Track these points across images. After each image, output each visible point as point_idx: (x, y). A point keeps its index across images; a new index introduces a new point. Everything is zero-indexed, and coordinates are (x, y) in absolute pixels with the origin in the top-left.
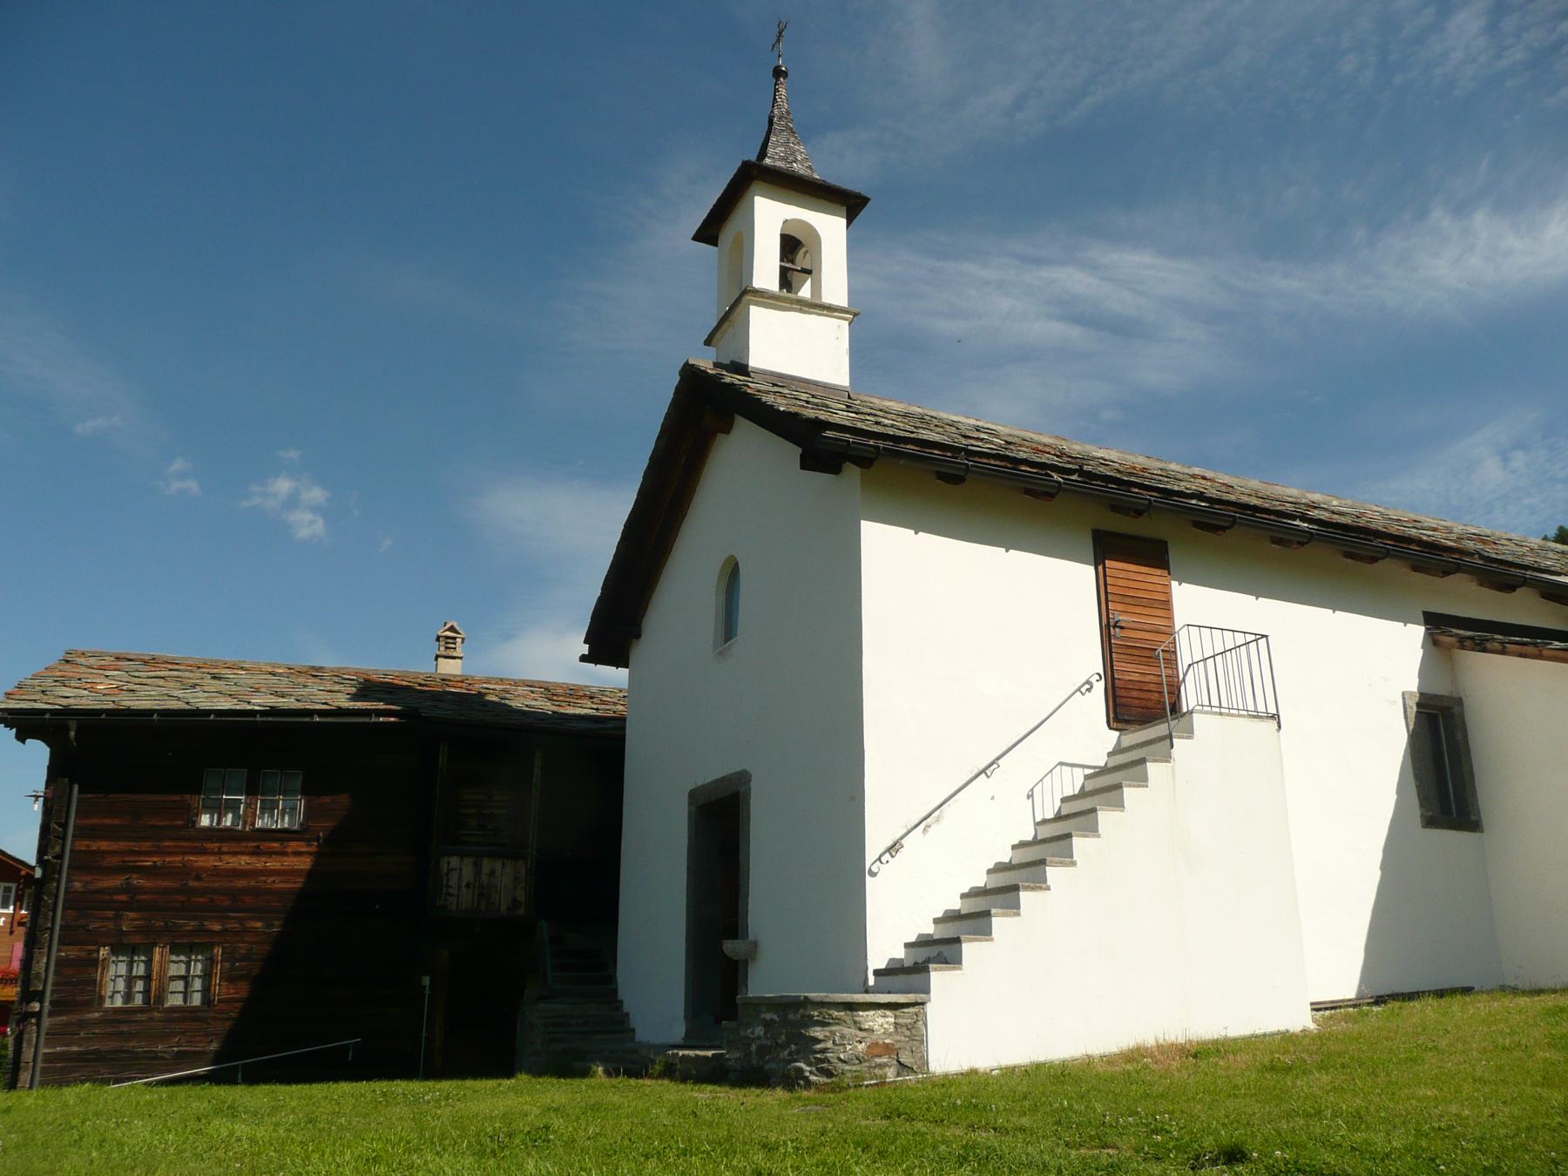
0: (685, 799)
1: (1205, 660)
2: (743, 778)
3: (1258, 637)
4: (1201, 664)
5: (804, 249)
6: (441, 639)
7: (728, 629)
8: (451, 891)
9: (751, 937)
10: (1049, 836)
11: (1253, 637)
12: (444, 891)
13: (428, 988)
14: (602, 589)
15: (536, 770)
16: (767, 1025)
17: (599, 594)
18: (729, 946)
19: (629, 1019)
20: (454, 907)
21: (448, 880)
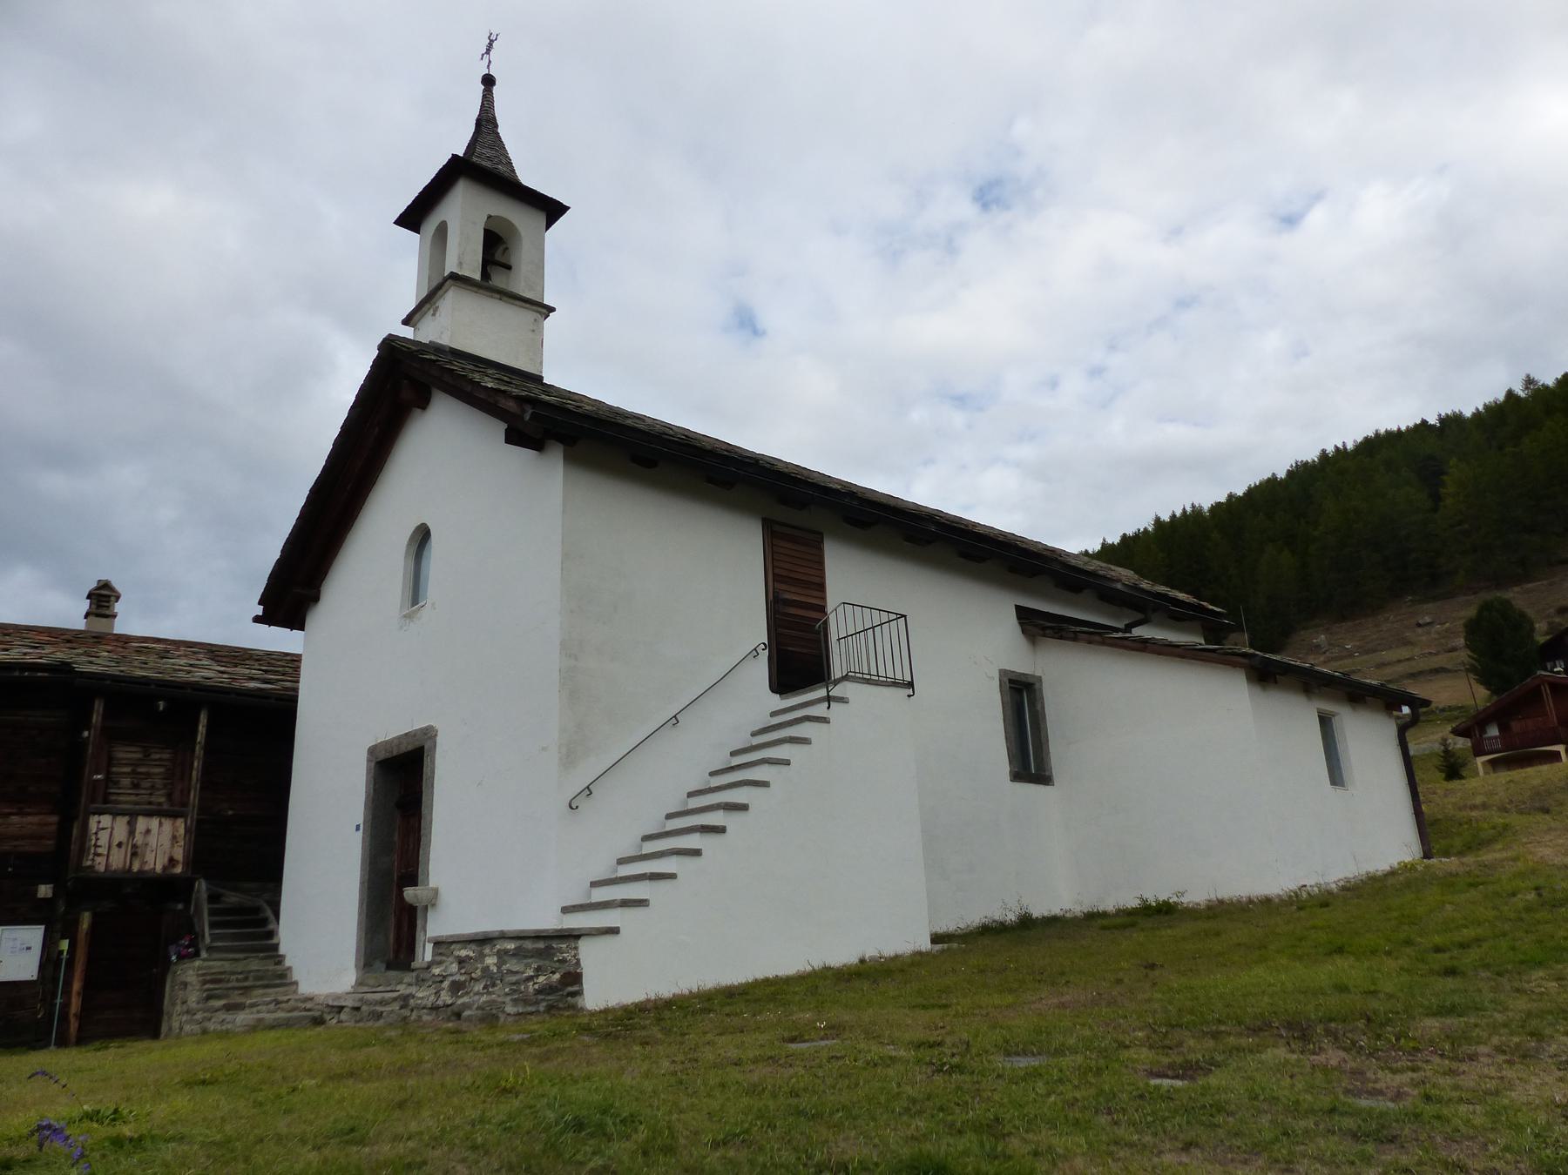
0: (364, 755)
1: (873, 628)
2: (429, 734)
3: (893, 617)
4: (870, 631)
5: (504, 246)
6: (93, 597)
7: (415, 592)
8: (100, 850)
9: (432, 884)
10: (703, 788)
11: (895, 617)
12: (92, 851)
13: (65, 953)
14: (282, 551)
15: (200, 728)
16: (461, 962)
17: (278, 557)
18: (409, 893)
19: (291, 971)
20: (102, 868)
21: (97, 839)
